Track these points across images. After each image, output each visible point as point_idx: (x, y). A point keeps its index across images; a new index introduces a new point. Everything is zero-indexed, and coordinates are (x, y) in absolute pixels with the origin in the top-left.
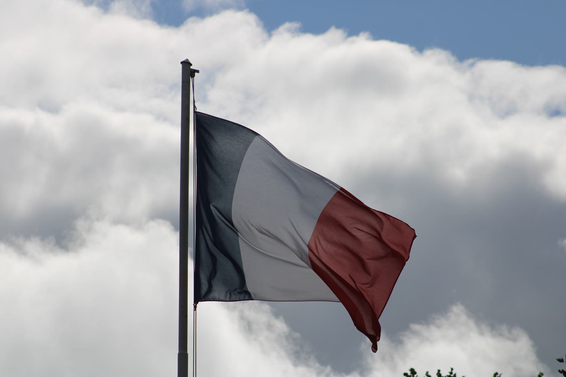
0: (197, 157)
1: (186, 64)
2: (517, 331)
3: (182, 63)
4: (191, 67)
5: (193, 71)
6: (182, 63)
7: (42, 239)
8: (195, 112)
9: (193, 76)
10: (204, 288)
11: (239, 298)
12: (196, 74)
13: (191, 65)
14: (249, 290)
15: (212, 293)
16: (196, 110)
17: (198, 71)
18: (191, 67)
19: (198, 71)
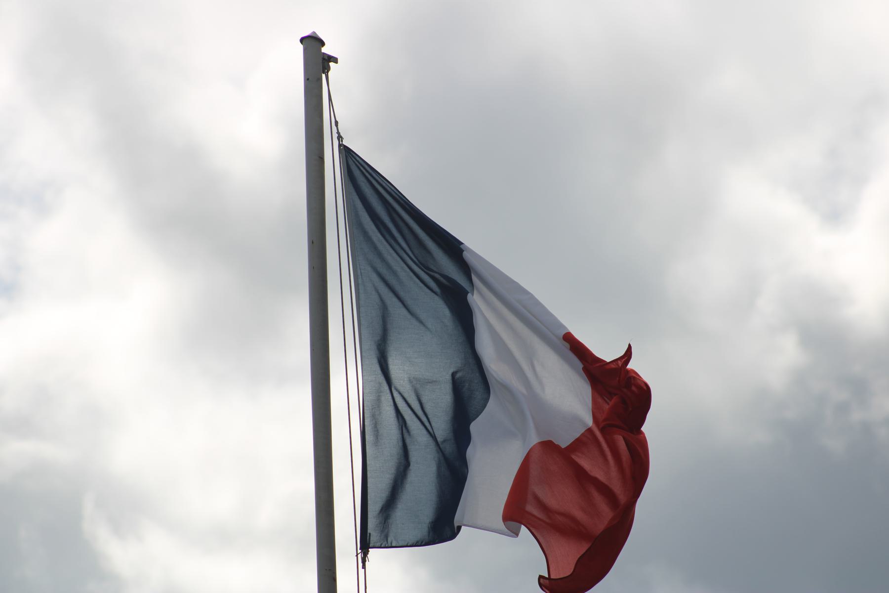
0: (349, 226)
1: (312, 42)
2: (642, 433)
3: (302, 40)
4: (324, 50)
5: (327, 58)
6: (302, 40)
7: (432, 522)
8: (340, 145)
9: (326, 69)
10: (374, 536)
11: (381, 544)
12: (331, 64)
13: (322, 43)
14: (471, 425)
15: (426, 529)
16: (342, 141)
17: (335, 60)
18: (324, 50)
19: (335, 60)
